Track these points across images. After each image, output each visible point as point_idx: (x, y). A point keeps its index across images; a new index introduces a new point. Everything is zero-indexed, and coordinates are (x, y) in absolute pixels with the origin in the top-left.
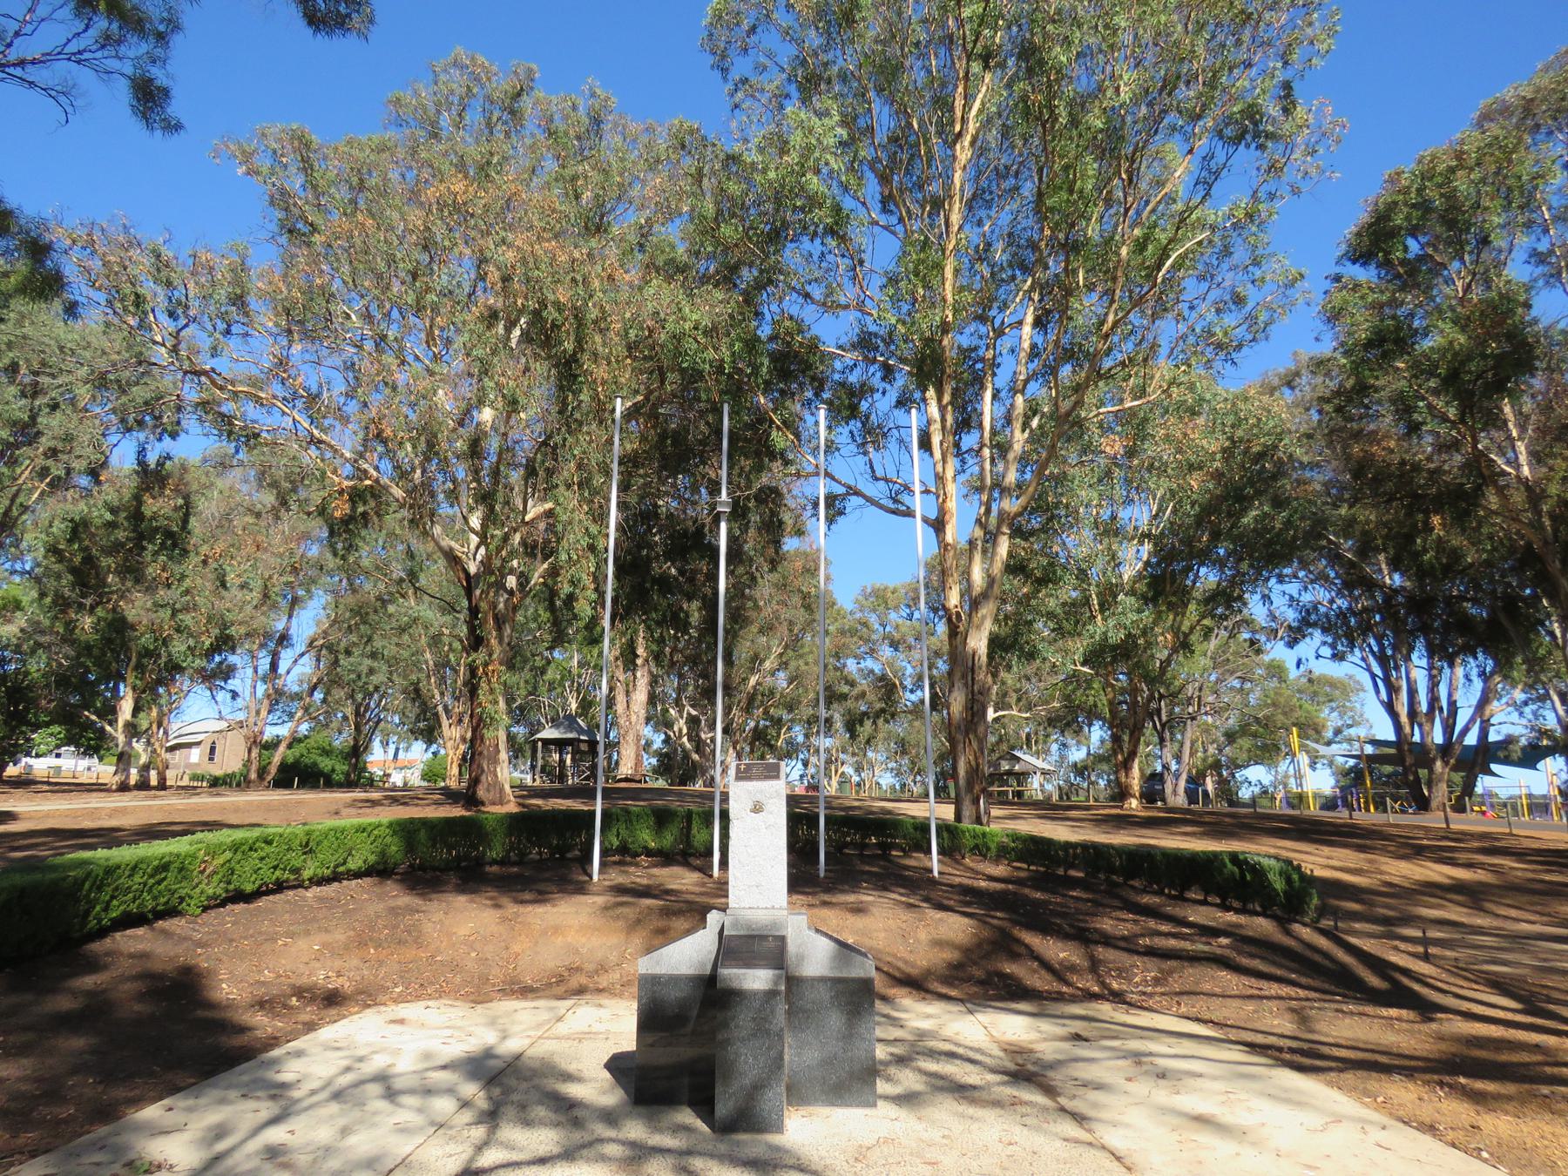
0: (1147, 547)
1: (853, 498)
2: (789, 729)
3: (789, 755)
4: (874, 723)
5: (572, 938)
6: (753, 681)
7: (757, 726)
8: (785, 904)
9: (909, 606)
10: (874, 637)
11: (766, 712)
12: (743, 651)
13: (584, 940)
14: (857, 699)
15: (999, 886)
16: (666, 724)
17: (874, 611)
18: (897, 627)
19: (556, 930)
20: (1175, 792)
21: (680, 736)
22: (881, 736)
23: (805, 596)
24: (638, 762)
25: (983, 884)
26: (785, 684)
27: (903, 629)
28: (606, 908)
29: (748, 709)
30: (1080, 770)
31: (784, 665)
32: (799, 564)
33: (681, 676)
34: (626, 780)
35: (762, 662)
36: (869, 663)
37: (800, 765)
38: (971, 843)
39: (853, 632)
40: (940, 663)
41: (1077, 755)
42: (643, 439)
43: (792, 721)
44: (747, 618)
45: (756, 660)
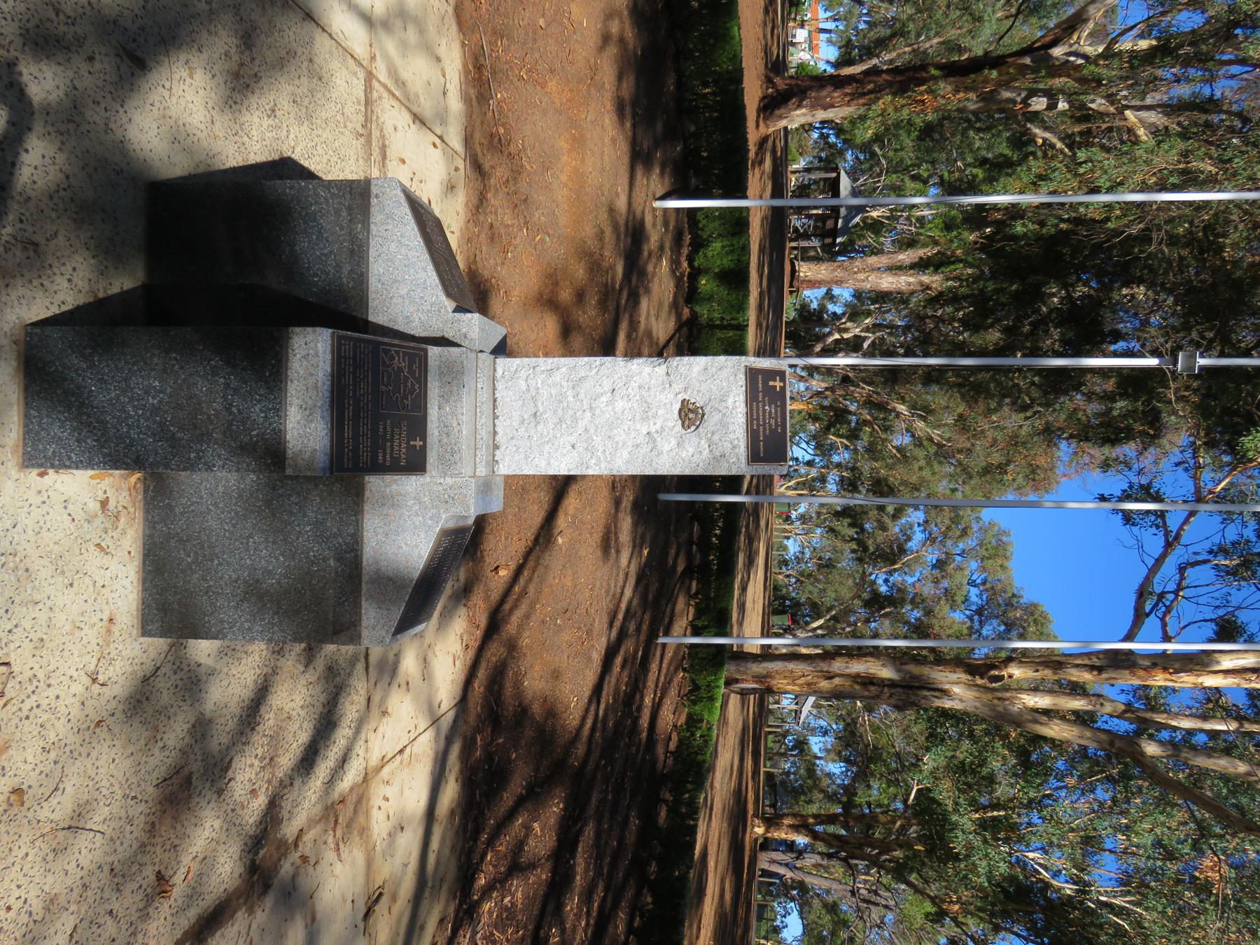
0: (1069, 889)
1: (1160, 541)
2: (847, 447)
3: (818, 447)
4: (852, 539)
5: (566, 162)
6: (902, 408)
7: (850, 413)
8: (510, 464)
9: (984, 583)
10: (949, 543)
11: (865, 423)
12: (937, 397)
13: (564, 178)
14: (878, 521)
15: (644, 721)
16: (854, 314)
17: (981, 545)
18: (960, 569)
19: (578, 142)
20: (773, 862)
21: (840, 331)
22: (839, 544)
23: (1002, 468)
24: (813, 284)
25: (648, 701)
26: (896, 442)
27: (958, 575)
28: (612, 211)
29: (869, 403)
30: (801, 745)
31: (918, 442)
32: (1042, 461)
33: (907, 328)
34: (793, 271)
35: (924, 419)
36: (918, 536)
37: (808, 457)
38: (702, 682)
39: (956, 520)
40: (917, 614)
41: (816, 744)
42: (1236, 263)
43: (855, 451)
44: (976, 402)
45: (926, 412)
